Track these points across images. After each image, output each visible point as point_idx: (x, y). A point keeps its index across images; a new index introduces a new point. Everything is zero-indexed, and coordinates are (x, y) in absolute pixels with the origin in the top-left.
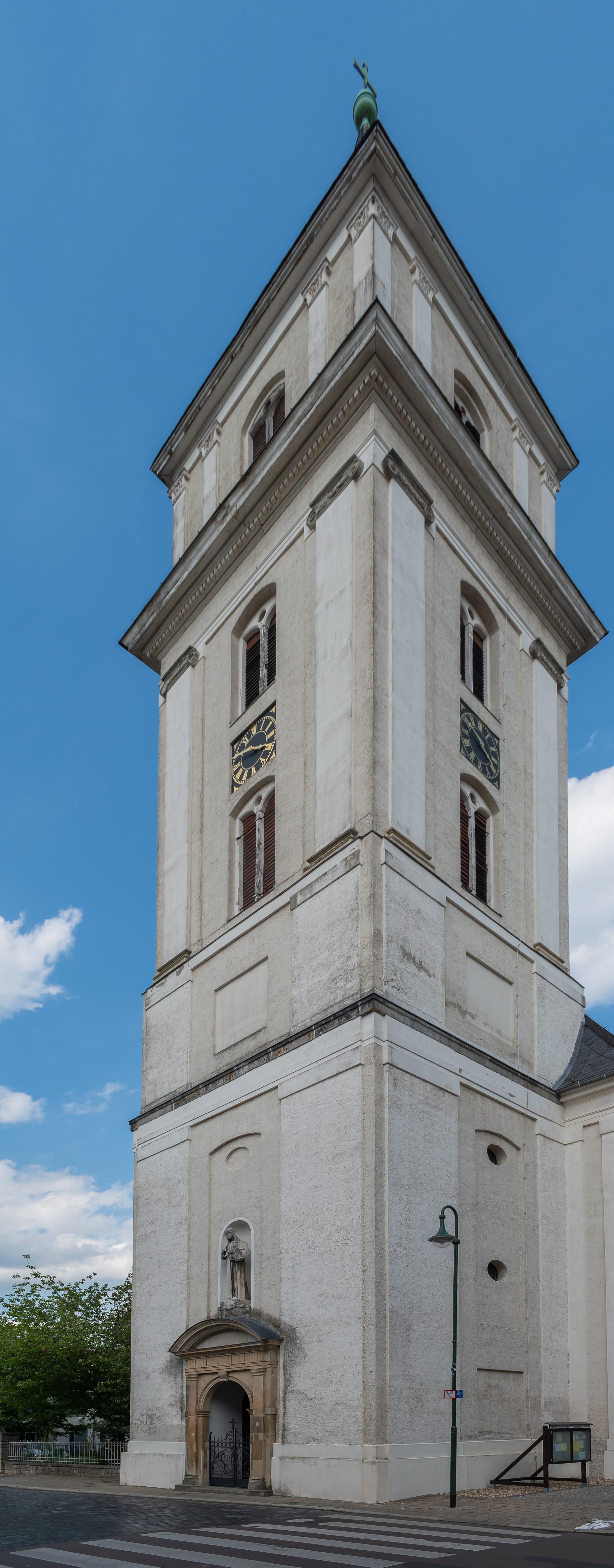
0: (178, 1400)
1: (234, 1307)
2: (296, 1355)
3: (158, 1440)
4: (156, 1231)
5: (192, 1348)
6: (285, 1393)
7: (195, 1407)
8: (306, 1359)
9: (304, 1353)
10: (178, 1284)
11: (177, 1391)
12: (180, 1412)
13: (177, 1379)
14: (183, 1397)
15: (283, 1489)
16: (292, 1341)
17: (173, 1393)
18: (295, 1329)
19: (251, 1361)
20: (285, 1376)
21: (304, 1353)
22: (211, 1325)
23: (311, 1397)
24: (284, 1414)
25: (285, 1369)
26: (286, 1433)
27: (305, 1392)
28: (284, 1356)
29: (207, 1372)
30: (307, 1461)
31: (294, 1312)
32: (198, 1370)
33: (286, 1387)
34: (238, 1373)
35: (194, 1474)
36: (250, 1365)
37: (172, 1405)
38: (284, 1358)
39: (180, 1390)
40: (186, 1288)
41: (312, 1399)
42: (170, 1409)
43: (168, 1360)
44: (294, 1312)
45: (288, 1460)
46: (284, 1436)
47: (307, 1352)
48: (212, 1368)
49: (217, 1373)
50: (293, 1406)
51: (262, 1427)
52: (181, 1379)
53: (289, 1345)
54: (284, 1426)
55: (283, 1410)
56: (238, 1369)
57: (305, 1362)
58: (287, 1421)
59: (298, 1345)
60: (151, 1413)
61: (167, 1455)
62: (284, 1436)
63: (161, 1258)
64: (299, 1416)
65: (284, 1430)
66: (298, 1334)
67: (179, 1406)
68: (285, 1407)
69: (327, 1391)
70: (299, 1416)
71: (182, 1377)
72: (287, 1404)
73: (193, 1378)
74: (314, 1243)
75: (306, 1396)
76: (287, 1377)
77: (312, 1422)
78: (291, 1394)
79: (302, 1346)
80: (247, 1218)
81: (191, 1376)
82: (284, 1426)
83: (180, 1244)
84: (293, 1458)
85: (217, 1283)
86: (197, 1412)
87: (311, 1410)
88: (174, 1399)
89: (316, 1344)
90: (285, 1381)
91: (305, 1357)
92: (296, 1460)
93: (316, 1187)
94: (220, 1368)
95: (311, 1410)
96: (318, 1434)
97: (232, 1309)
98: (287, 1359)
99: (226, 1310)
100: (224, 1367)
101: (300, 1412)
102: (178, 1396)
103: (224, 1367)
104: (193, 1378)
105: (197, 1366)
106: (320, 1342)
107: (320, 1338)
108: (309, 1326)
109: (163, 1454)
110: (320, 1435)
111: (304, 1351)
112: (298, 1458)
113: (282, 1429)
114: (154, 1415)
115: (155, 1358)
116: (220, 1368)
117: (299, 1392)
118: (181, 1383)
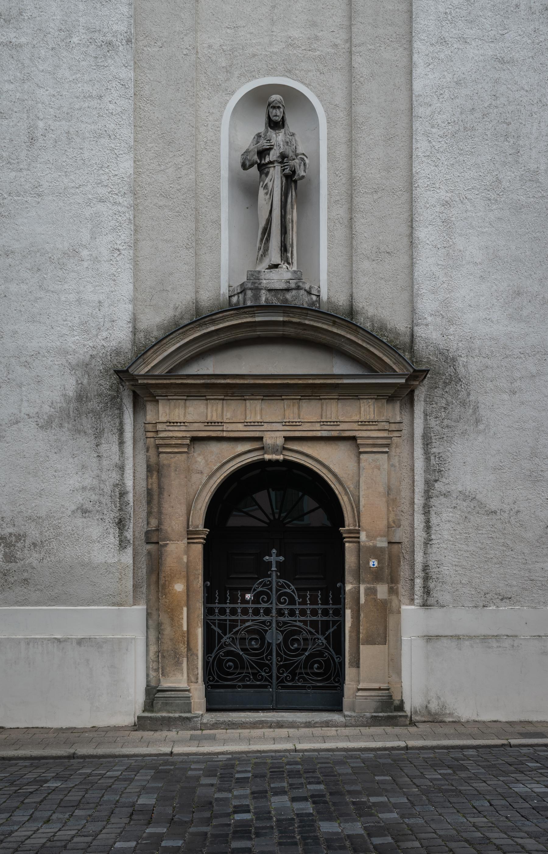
0: (106, 500)
1: (293, 285)
2: (455, 416)
3: (37, 604)
4: (21, 46)
5: (170, 373)
6: (428, 496)
7: (183, 519)
8: (481, 427)
9: (474, 412)
10: (101, 201)
11: (104, 476)
12: (114, 531)
13: (104, 447)
14: (122, 494)
15: (434, 707)
16: (446, 384)
17: (88, 481)
18: (454, 360)
19: (356, 418)
20: (427, 459)
21: (474, 412)
22: (258, 319)
23: (493, 508)
24: (428, 542)
25: (427, 443)
26: (432, 585)
27: (479, 497)
28: (426, 415)
29: (225, 434)
30: (494, 644)
31: (451, 322)
32: (195, 426)
33: (429, 485)
34: (310, 444)
35: (183, 685)
36: (355, 426)
37: (85, 512)
38: (426, 420)
39: (115, 476)
40: (130, 215)
41: (495, 512)
42: (79, 521)
43: (71, 393)
44: (451, 322)
45: (445, 640)
46: (427, 591)
47: (482, 412)
48: (240, 427)
49: (260, 439)
50: (448, 526)
51: (387, 571)
52: (115, 448)
53: (439, 392)
54: (425, 568)
55: (424, 535)
56: (319, 434)
57: (479, 432)
58: (433, 557)
59: (463, 394)
60: (11, 530)
61: (80, 642)
62: (427, 591)
63: (41, 124)
64: (465, 547)
65: (426, 578)
66: (462, 371)
67: (111, 515)
68: (428, 527)
69: (530, 496)
70: (465, 547)
71: (121, 443)
72: (434, 520)
73: (181, 445)
74: (499, 181)
75: (481, 504)
76: (433, 462)
77: (495, 560)
78: (443, 499)
79: (472, 398)
80: (308, 85)
81: (173, 442)
82: (425, 568)
83: (106, 99)
84: (458, 638)
85: (217, 223)
86: (189, 532)
87: (494, 535)
88: (94, 497)
89: (506, 397)
90: (427, 469)
91: (478, 421)
92: (467, 643)
93: (502, 61)
94: (266, 427)
95: (494, 535)
96: (511, 586)
97: (288, 290)
98: (433, 423)
99: (270, 290)
100: (279, 427)
101: (466, 538)
102: (108, 489)
103: (279, 427)
104: (181, 445)
105: (189, 418)
106: (514, 393)
107: (517, 384)
108: (487, 357)
109: (66, 640)
110: (515, 589)
111: (476, 409)
112: (470, 637)
113: (422, 574)
114: (19, 537)
115: (20, 386)
116: (266, 427)
117: (465, 496)
118: (116, 459)
